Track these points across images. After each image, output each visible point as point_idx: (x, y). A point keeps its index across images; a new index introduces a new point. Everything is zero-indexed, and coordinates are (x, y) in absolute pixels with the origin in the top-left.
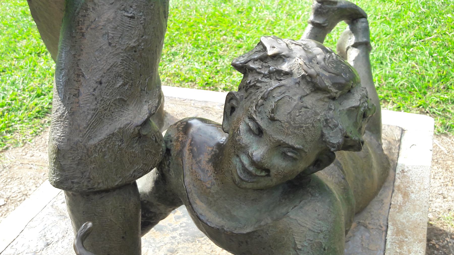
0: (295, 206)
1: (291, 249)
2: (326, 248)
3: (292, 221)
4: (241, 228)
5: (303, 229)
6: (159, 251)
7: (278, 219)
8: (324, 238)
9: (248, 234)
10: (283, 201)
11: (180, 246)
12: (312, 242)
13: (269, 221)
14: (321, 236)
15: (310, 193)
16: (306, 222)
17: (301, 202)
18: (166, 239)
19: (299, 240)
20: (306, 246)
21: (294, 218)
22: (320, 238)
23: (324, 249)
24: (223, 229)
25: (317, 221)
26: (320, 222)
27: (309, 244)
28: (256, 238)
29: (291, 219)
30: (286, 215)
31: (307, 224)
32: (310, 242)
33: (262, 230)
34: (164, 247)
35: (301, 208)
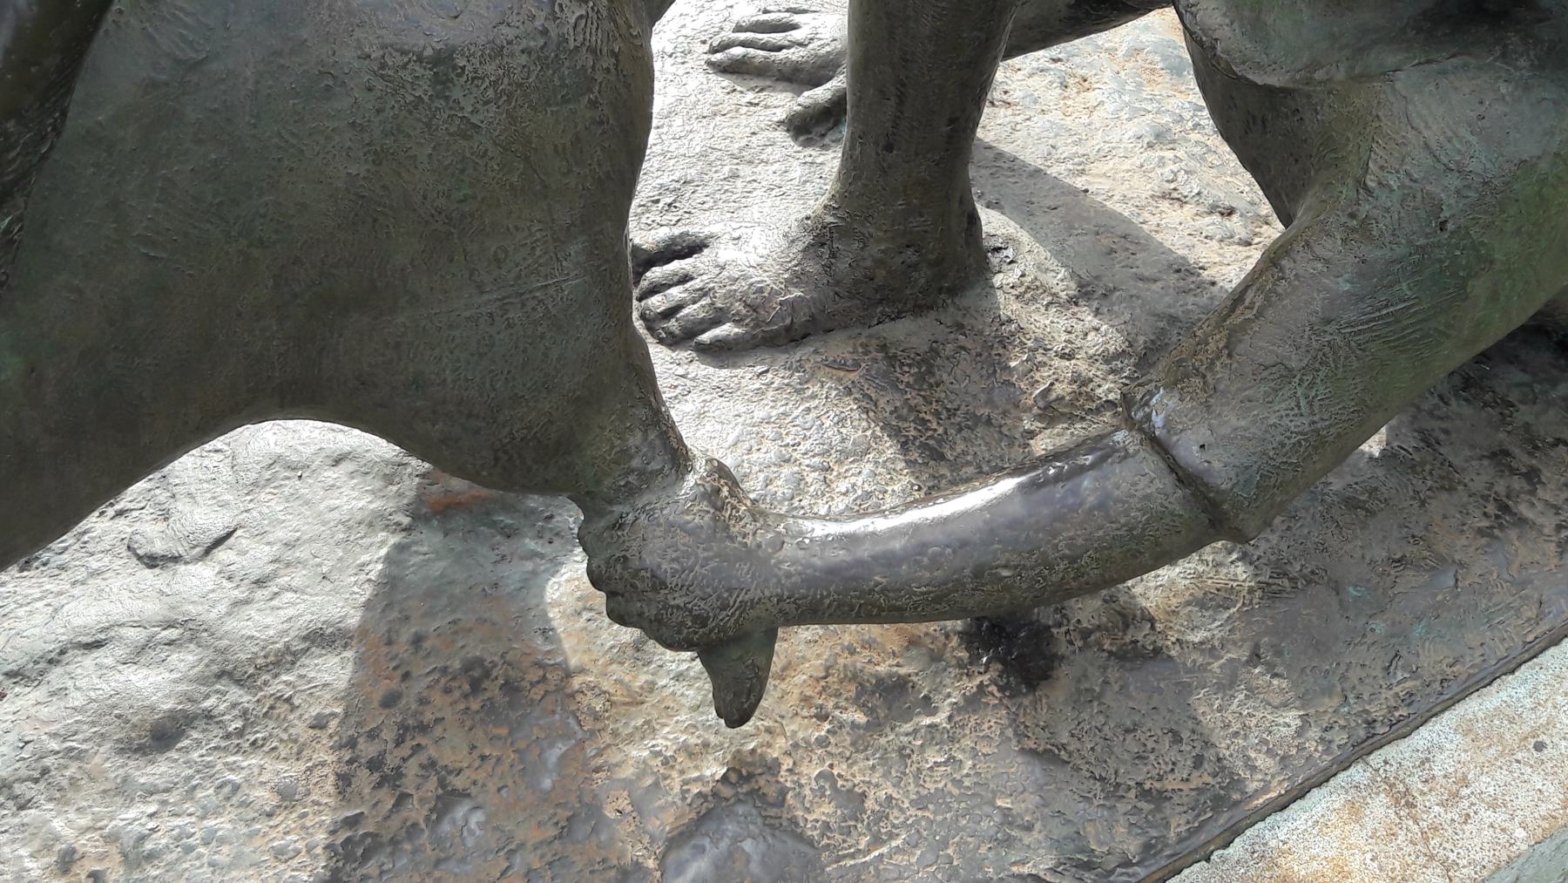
0: (1428, 62)
1: (1350, 181)
2: (1450, 226)
3: (1392, 99)
4: (1259, 67)
5: (1411, 135)
6: (1129, 120)
7: (1365, 77)
8: (1458, 192)
9: (1269, 90)
10: (1411, 34)
11: (1194, 136)
12: (1414, 185)
13: (1340, 75)
14: (1454, 181)
15: (1505, 46)
16: (1430, 120)
17: (1454, 56)
18: (1172, 100)
19: (1382, 162)
20: (1392, 191)
21: (1404, 93)
22: (1445, 189)
23: (1442, 226)
24: (1214, 48)
25: (1463, 132)
26: (1474, 139)
27: (1402, 187)
28: (1287, 117)
29: (1394, 90)
30: (1387, 75)
31: (1427, 127)
32: (1408, 183)
33: (1309, 96)
34: (1150, 116)
35: (1444, 73)
